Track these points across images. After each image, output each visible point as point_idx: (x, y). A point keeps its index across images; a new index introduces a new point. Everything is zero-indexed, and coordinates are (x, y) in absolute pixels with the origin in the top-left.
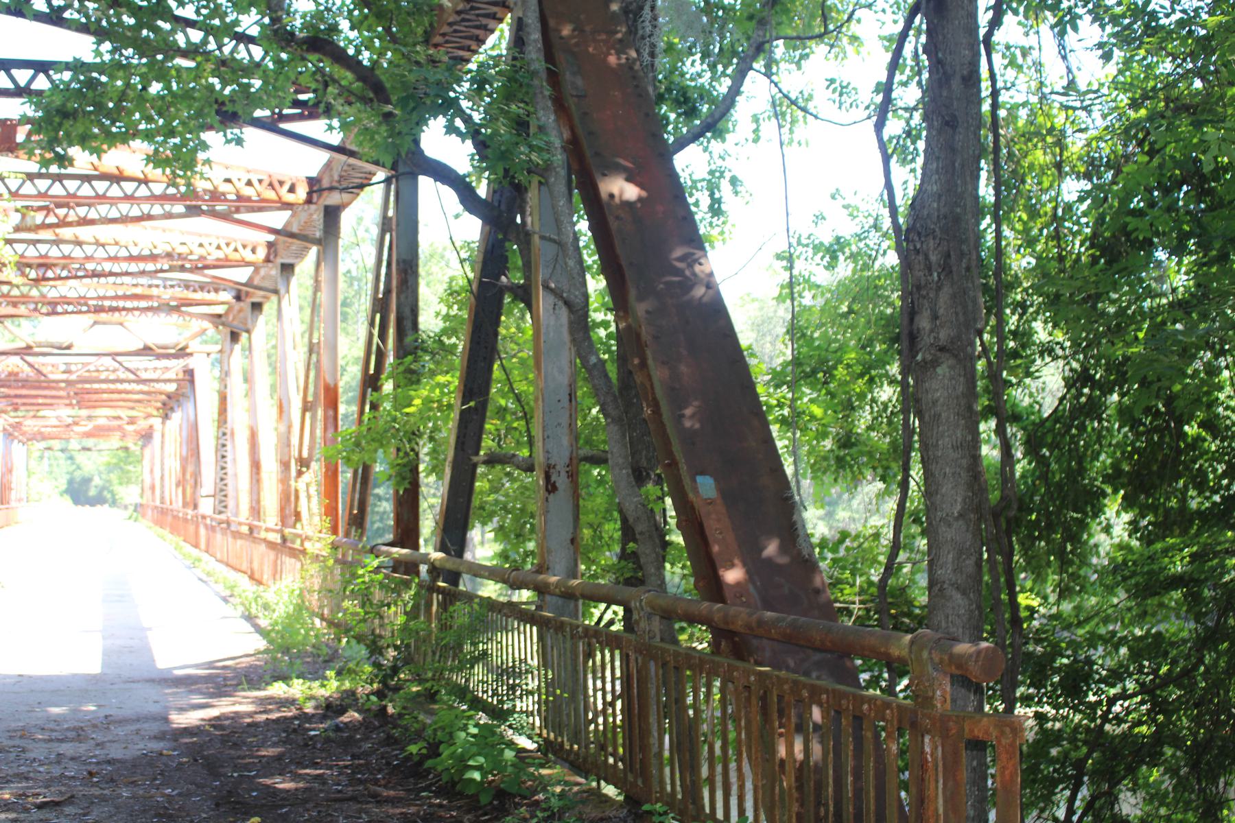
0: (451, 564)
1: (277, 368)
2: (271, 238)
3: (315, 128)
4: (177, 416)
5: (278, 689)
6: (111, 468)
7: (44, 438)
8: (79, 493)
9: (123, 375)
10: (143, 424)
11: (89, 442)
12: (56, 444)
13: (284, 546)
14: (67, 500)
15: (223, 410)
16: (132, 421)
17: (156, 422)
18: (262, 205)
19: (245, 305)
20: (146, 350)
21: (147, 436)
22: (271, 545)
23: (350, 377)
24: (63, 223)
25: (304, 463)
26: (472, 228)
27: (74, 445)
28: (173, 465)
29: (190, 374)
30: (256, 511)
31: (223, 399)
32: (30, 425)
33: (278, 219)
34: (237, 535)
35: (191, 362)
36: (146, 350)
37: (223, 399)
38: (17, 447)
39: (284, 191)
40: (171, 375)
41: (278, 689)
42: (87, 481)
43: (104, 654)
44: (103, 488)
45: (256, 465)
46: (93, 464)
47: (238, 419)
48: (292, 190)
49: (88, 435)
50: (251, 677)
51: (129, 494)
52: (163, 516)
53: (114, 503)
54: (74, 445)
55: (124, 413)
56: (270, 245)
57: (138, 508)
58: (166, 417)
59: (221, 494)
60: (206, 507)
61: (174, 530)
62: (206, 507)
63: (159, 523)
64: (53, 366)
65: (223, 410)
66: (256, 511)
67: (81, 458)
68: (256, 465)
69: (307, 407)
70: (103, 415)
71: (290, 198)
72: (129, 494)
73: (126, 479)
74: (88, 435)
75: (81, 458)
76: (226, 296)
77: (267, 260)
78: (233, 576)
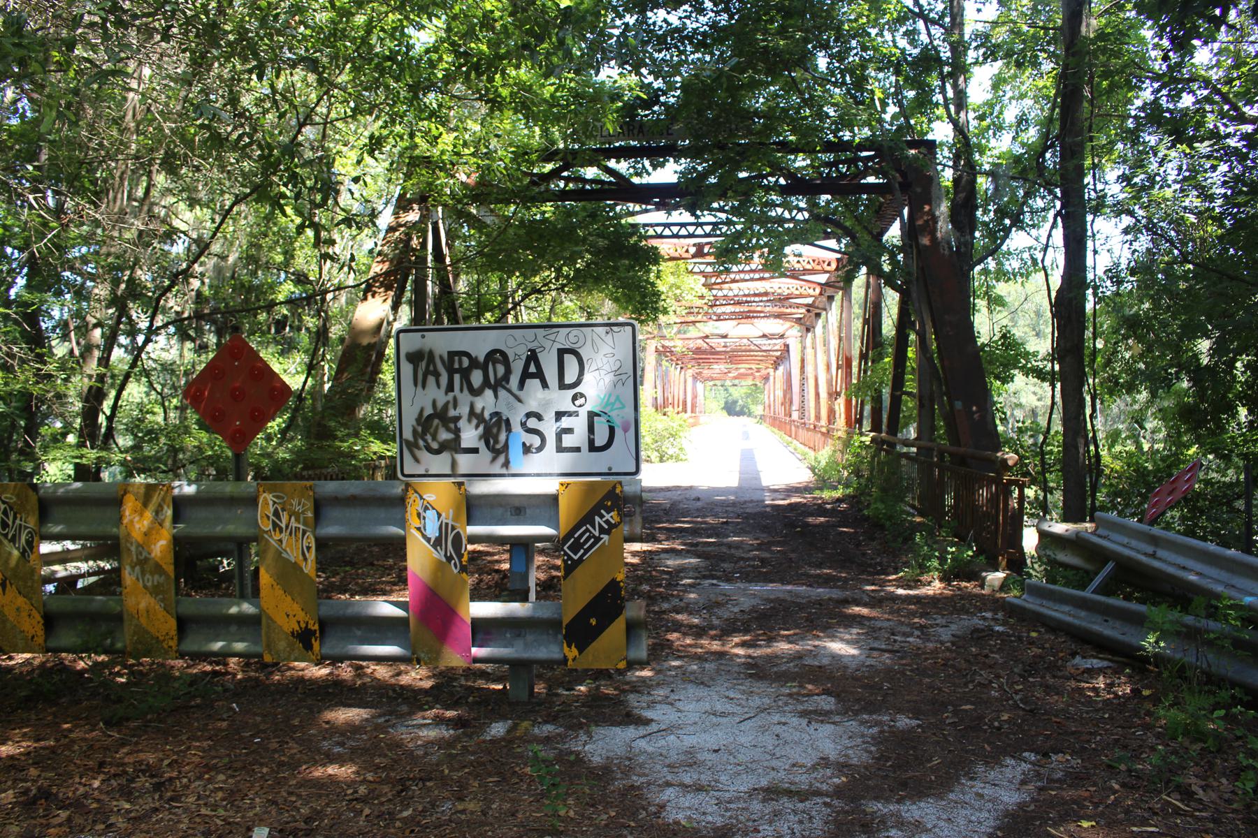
0: (891, 439)
1: (826, 343)
2: (839, 256)
3: (832, 243)
4: (781, 368)
5: (817, 494)
6: (748, 395)
7: (713, 379)
8: (731, 409)
9: (753, 347)
10: (764, 372)
11: (736, 382)
12: (718, 383)
13: (828, 434)
14: (725, 413)
15: (803, 367)
16: (758, 370)
17: (771, 371)
18: (813, 272)
19: (812, 314)
20: (764, 336)
21: (766, 378)
22: (823, 434)
23: (856, 353)
24: (724, 283)
25: (838, 394)
26: (896, 296)
27: (728, 383)
28: (780, 393)
29: (787, 346)
30: (818, 418)
31: (803, 361)
32: (706, 373)
33: (823, 278)
34: (808, 430)
35: (788, 341)
36: (764, 336)
37: (803, 361)
38: (700, 386)
39: (825, 266)
40: (777, 347)
41: (817, 494)
42: (735, 402)
43: (742, 460)
44: (743, 407)
45: (817, 395)
46: (738, 393)
47: (809, 369)
48: (829, 264)
49: (735, 378)
50: (806, 489)
51: (758, 410)
52: (776, 422)
53: (750, 414)
54: (728, 383)
55: (753, 366)
56: (838, 260)
57: (762, 417)
58: (776, 369)
59: (802, 409)
60: (795, 416)
61: (780, 429)
62: (795, 416)
63: (773, 425)
64: (717, 343)
65: (803, 367)
66: (818, 418)
67: (732, 390)
68: (817, 395)
69: (838, 367)
70: (743, 368)
71: (828, 268)
72: (758, 410)
73: (756, 402)
74: (735, 378)
75: (732, 390)
76: (803, 310)
77: (821, 294)
78: (807, 450)
